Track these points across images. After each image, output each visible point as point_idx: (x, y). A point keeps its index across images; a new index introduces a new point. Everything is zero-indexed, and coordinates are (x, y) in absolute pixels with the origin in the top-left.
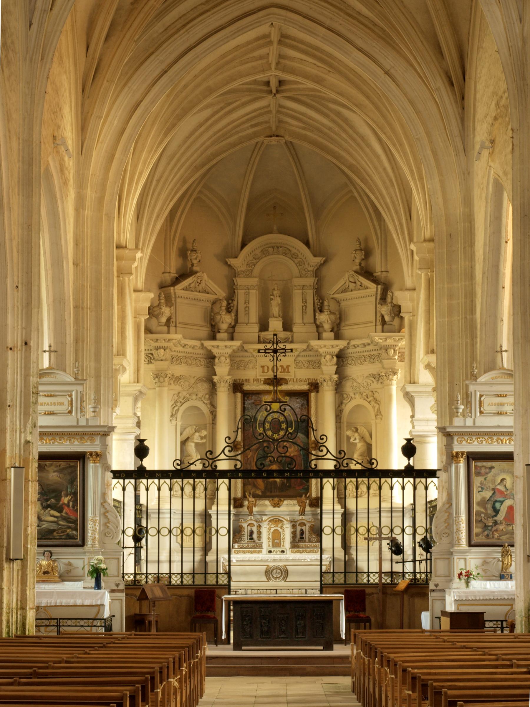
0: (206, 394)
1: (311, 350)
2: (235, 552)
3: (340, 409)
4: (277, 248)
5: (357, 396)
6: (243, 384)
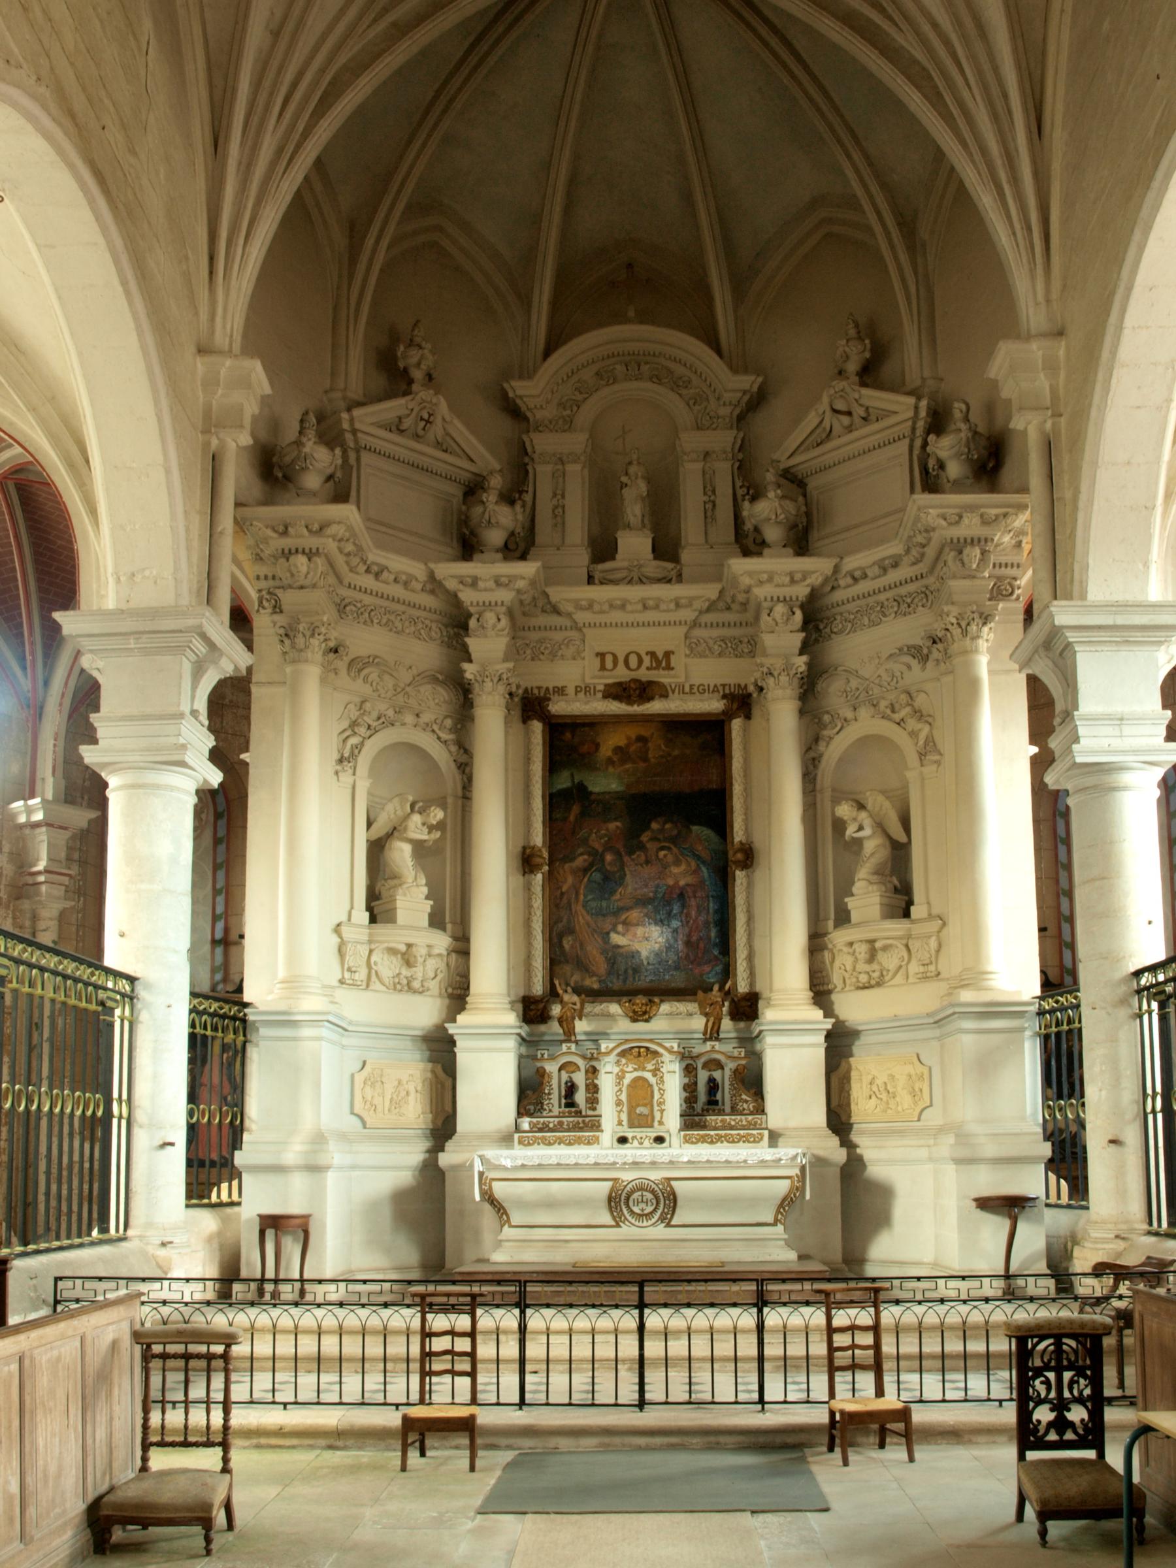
0: (446, 717)
1: (728, 608)
2: (520, 1142)
3: (812, 754)
4: (638, 365)
5: (864, 713)
6: (549, 699)
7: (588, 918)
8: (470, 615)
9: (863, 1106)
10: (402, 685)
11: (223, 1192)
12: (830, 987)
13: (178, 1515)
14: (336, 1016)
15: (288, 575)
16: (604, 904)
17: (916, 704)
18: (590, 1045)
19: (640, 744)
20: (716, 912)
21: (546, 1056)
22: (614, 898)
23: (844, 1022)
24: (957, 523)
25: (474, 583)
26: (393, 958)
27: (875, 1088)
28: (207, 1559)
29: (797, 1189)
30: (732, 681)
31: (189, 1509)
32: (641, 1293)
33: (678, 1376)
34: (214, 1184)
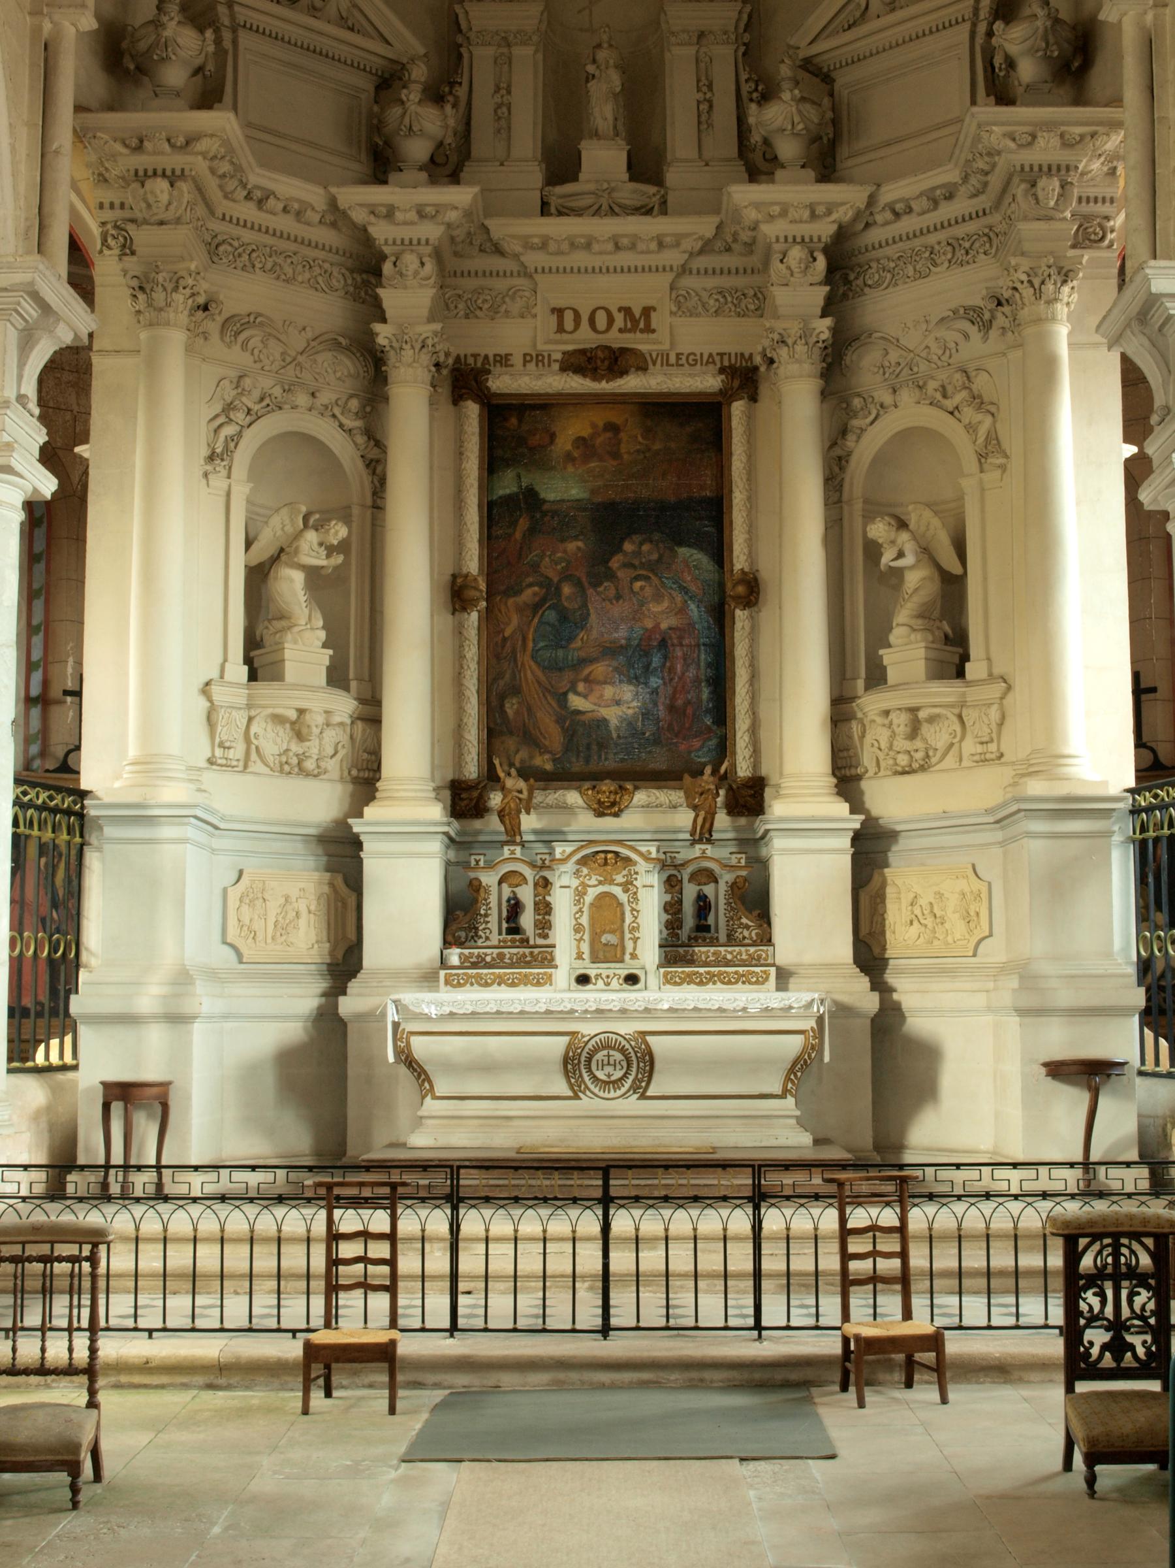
0: (351, 396)
1: (728, 249)
2: (447, 983)
3: (837, 451)
5: (907, 396)
6: (489, 372)
7: (539, 673)
8: (383, 257)
9: (901, 934)
10: (293, 354)
11: (49, 1053)
12: (860, 771)
13: (37, 1458)
14: (206, 810)
15: (144, 205)
16: (560, 653)
17: (974, 387)
18: (541, 848)
19: (609, 435)
20: (709, 665)
21: (482, 864)
22: (573, 646)
23: (877, 819)
24: (1030, 144)
25: (389, 213)
26: (280, 729)
27: (918, 912)
28: (75, 1512)
29: (813, 1048)
30: (733, 349)
31: (51, 1450)
32: (606, 1186)
33: (652, 1300)
34: (41, 1041)
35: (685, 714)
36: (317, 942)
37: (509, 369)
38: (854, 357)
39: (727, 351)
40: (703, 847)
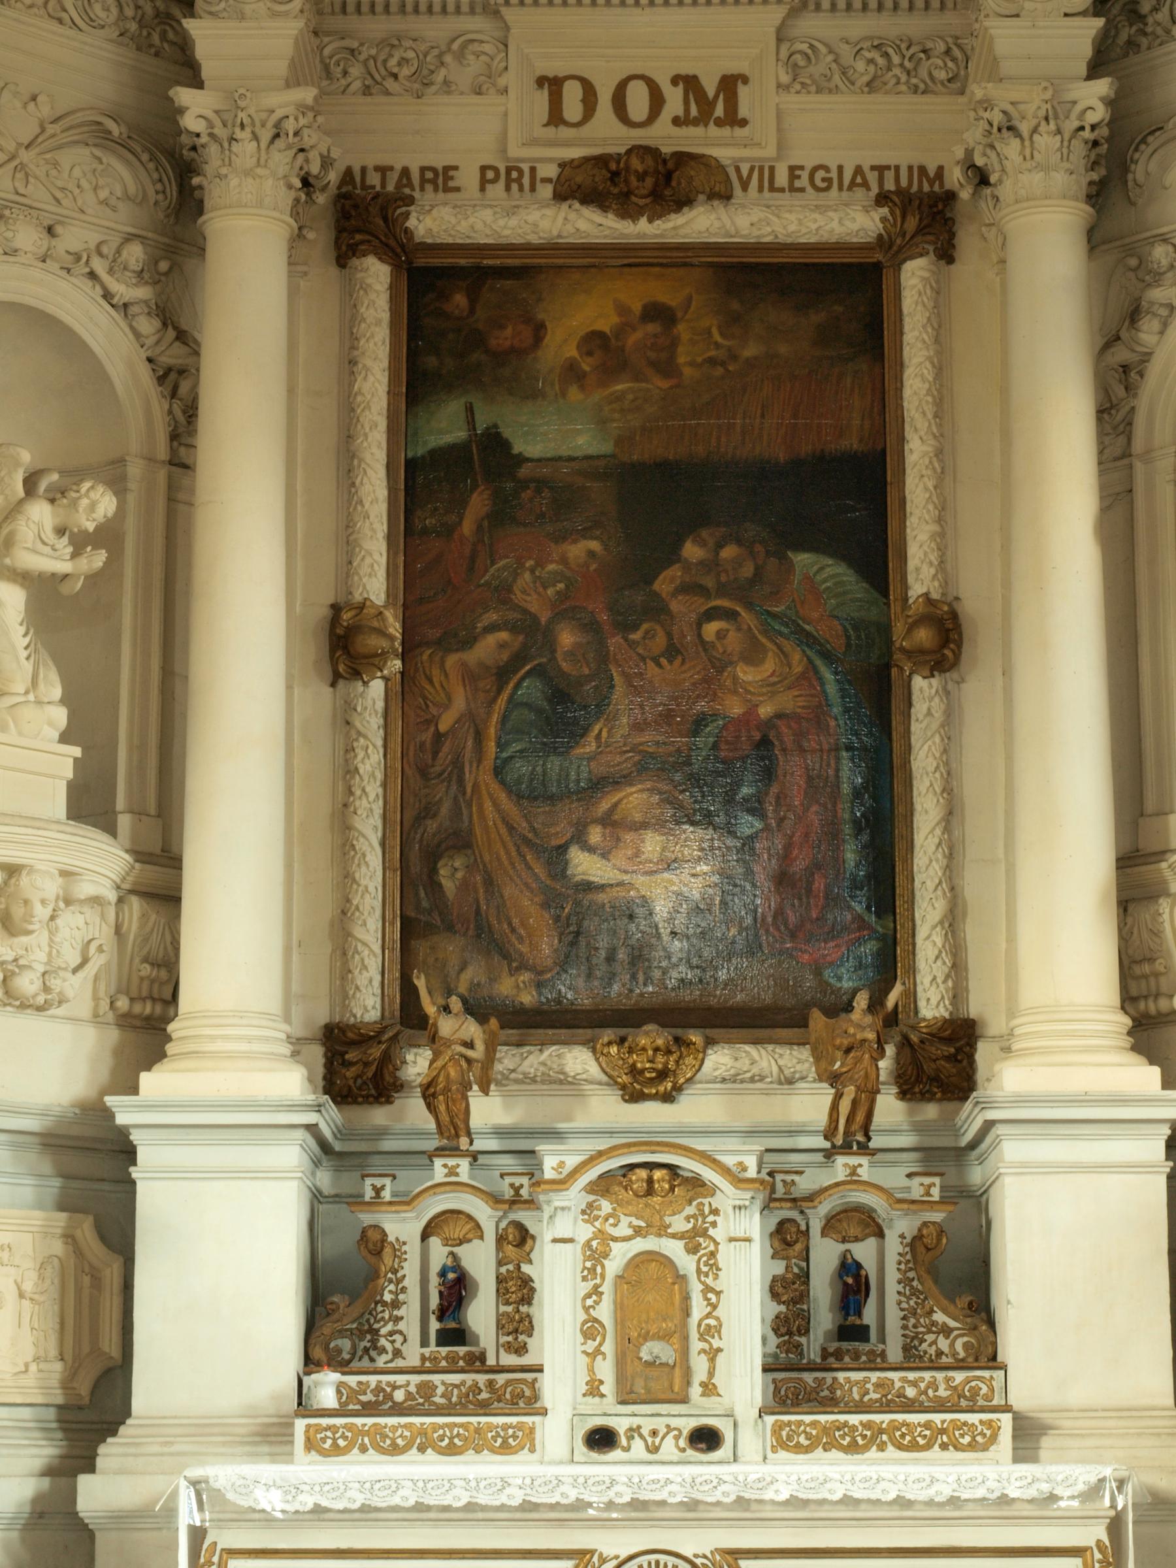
0: (129, 238)
2: (310, 1445)
6: (410, 201)
10: (11, 146)
16: (554, 764)
19: (652, 328)
21: (387, 1195)
30: (903, 157)
35: (809, 891)
36: (36, 1359)
37: (450, 196)
38: (1153, 166)
39: (892, 162)
40: (853, 1160)
